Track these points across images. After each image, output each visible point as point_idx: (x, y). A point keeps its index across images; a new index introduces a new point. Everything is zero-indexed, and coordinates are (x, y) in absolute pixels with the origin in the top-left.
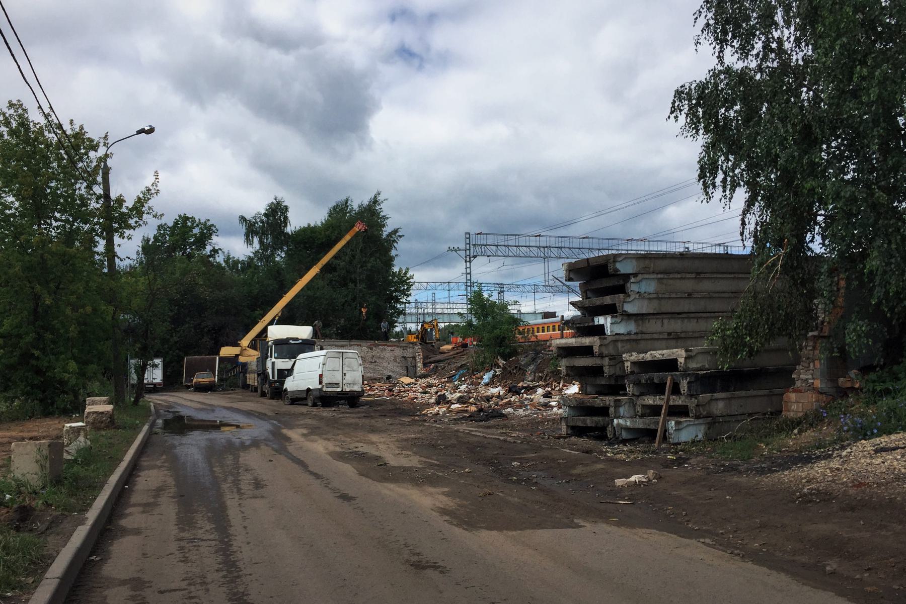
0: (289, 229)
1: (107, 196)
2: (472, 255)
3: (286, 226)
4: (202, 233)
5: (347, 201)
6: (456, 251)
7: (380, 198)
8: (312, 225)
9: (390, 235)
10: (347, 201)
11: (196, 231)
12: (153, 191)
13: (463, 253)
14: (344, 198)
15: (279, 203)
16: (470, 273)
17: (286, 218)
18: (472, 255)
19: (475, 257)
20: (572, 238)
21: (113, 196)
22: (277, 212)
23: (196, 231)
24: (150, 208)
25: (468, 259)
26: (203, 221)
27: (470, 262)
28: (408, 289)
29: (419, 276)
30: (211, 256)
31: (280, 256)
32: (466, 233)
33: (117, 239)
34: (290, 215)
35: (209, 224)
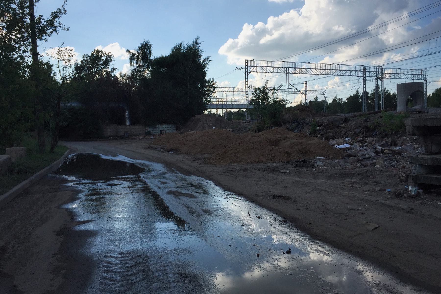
0: (152, 58)
1: (32, 14)
2: (249, 71)
3: (150, 56)
4: (106, 59)
5: (181, 44)
6: (240, 69)
7: (199, 41)
8: (164, 56)
9: (205, 60)
10: (181, 44)
11: (104, 58)
12: (62, 11)
13: (244, 71)
14: (179, 43)
15: (147, 44)
16: (248, 81)
17: (150, 52)
18: (249, 71)
19: (250, 72)
20: (302, 63)
21: (36, 15)
22: (145, 49)
23: (104, 58)
24: (60, 24)
25: (247, 74)
26: (107, 53)
27: (248, 75)
28: (214, 90)
29: (219, 83)
30: (112, 71)
31: (147, 73)
32: (246, 60)
33: (39, 42)
34: (153, 50)
35: (110, 54)
